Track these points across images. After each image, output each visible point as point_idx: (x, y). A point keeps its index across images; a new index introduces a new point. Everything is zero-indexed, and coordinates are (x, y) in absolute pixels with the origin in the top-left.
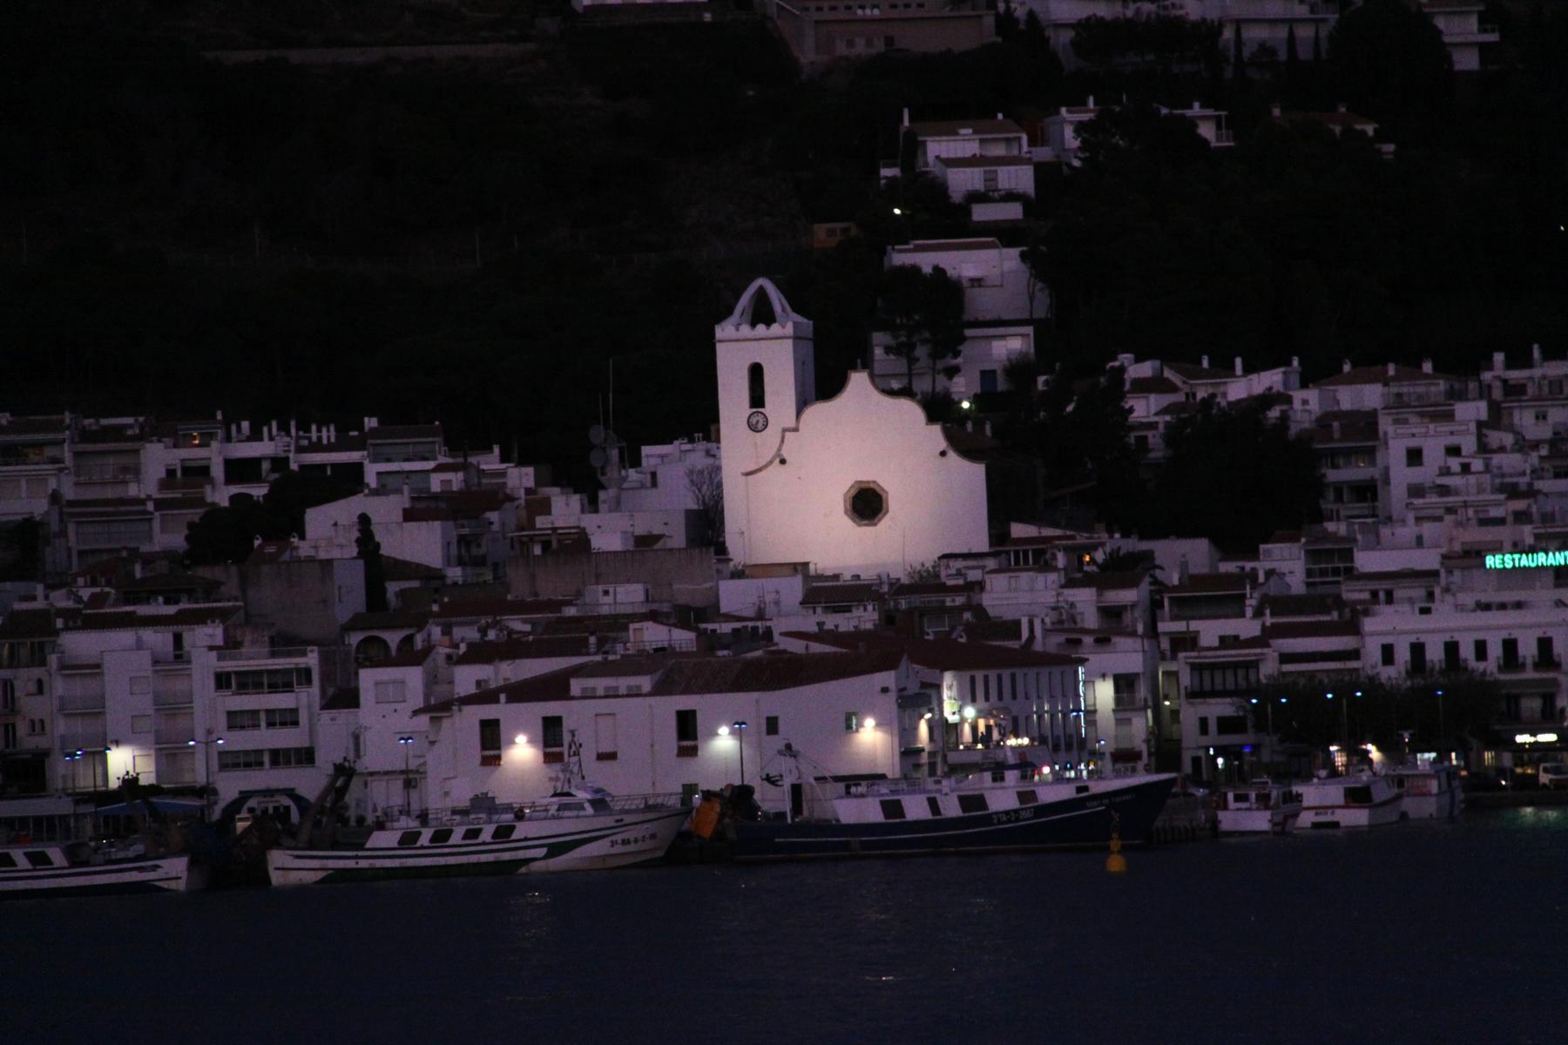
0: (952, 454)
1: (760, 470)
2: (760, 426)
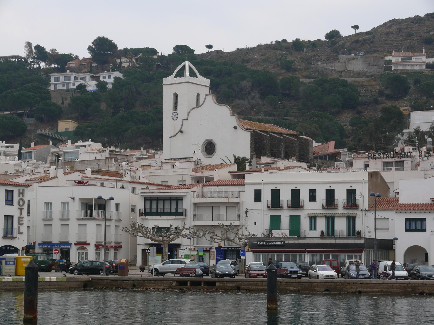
0: (239, 129)
1: (175, 136)
2: (176, 118)
